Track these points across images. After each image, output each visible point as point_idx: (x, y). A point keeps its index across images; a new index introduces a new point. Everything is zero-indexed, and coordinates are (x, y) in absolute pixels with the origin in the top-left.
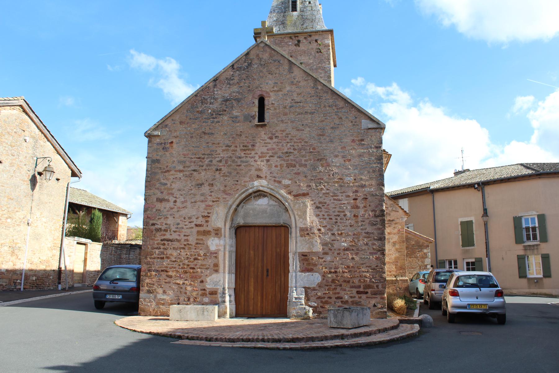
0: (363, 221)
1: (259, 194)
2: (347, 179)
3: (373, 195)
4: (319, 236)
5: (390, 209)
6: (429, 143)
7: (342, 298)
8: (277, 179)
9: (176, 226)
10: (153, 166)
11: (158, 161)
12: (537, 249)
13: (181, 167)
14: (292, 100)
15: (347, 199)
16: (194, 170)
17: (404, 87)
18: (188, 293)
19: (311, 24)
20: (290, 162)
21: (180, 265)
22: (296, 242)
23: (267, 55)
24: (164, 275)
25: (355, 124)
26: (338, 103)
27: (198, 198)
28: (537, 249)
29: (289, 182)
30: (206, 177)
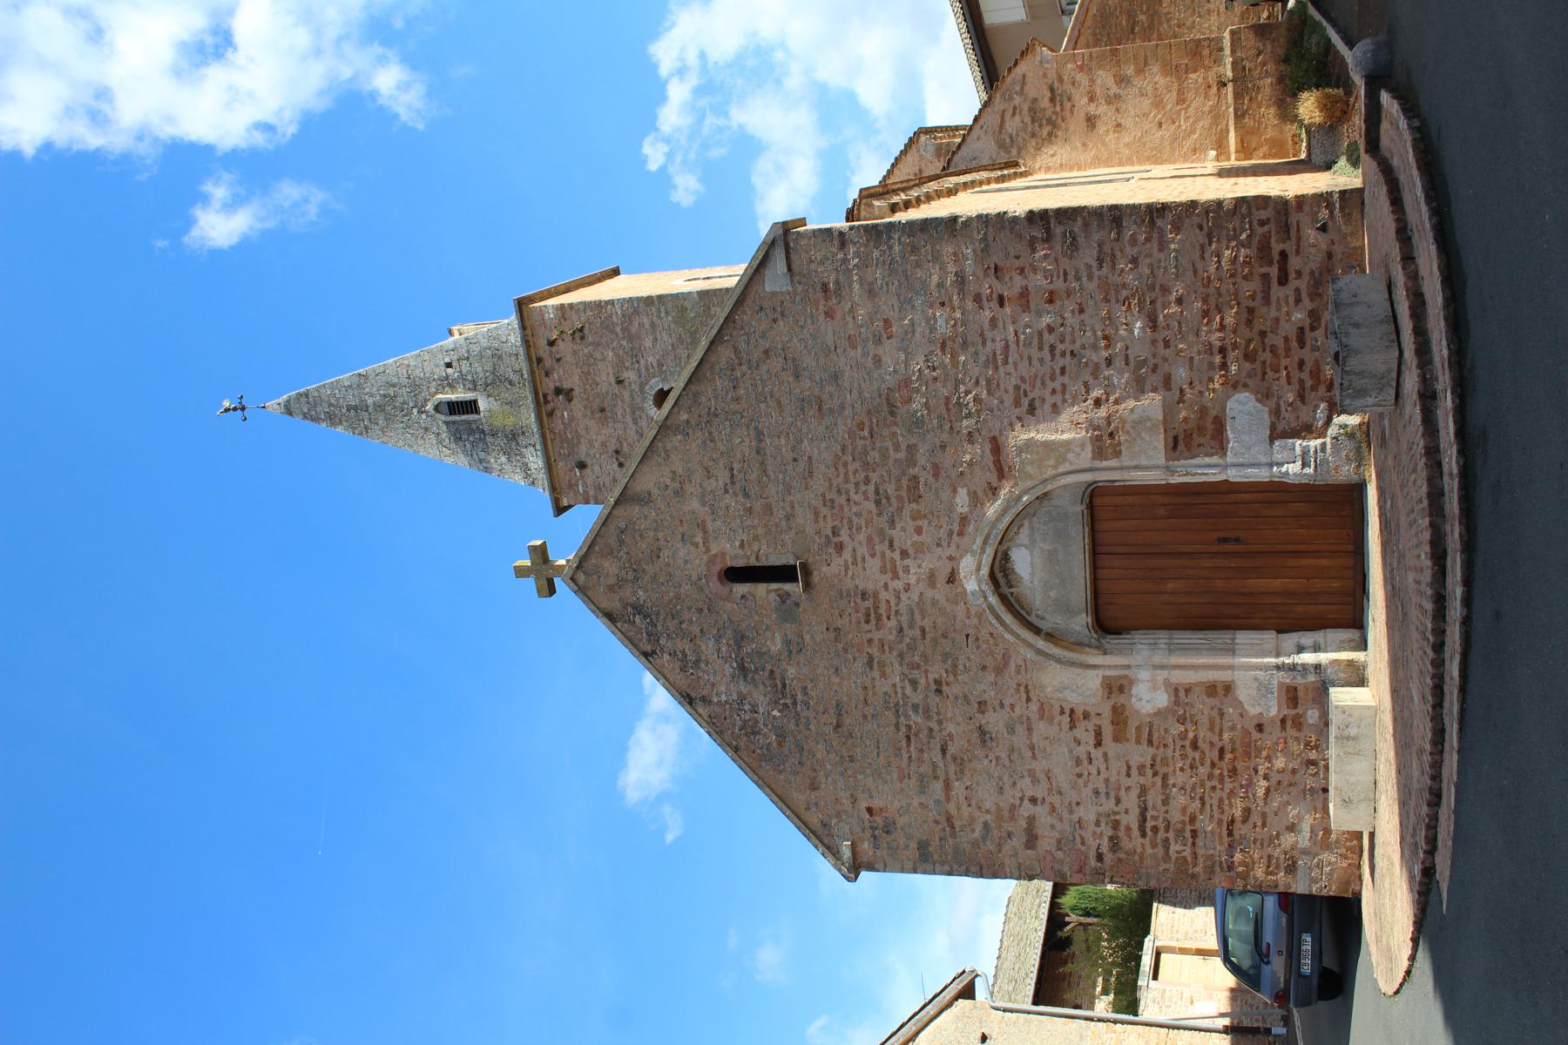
0: (1065, 274)
1: (1000, 574)
4: (1116, 402)
5: (1017, 100)
7: (1301, 329)
8: (956, 527)
9: (1103, 796)
10: (936, 857)
11: (923, 846)
13: (938, 786)
14: (727, 491)
15: (1001, 324)
16: (944, 751)
19: (507, 360)
20: (904, 493)
21: (1214, 788)
22: (1137, 467)
23: (606, 564)
24: (1241, 830)
26: (723, 364)
27: (1020, 740)
30: (960, 719)
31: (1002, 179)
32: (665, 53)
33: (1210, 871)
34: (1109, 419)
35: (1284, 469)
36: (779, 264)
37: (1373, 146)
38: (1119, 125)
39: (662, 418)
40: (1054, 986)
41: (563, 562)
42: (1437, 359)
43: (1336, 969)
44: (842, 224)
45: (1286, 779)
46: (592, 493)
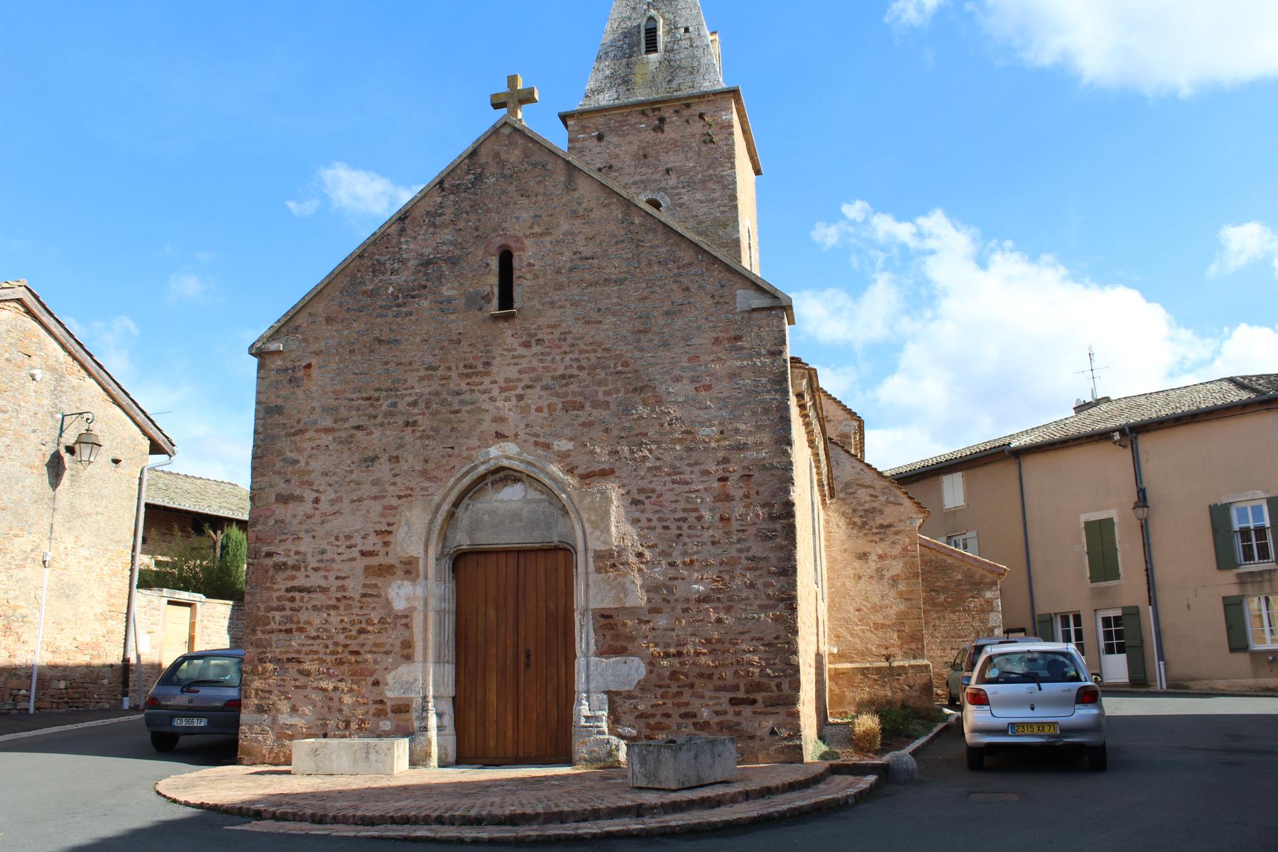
0: (743, 531)
1: (502, 475)
2: (704, 432)
3: (764, 468)
4: (640, 570)
5: (882, 498)
6: (957, 336)
7: (695, 716)
8: (542, 440)
9: (320, 557)
10: (269, 421)
11: (279, 410)
12: (1270, 580)
13: (328, 422)
14: (575, 253)
15: (704, 478)
16: (358, 428)
17: (958, 216)
18: (346, 711)
19: (689, 78)
20: (570, 398)
21: (327, 647)
22: (587, 586)
23: (517, 152)
24: (292, 669)
25: (722, 300)
26: (679, 254)
27: (367, 490)
28: (1270, 580)
29: (569, 446)
30: (384, 441)
31: (821, 485)
32: (936, 222)
33: (258, 644)
34: (626, 564)
35: (584, 702)
36: (758, 301)
37: (836, 770)
38: (860, 578)
39: (637, 202)
40: (162, 521)
41: (520, 115)
42: (668, 817)
43: (177, 747)
44: (789, 353)
45: (335, 704)
46: (578, 145)
